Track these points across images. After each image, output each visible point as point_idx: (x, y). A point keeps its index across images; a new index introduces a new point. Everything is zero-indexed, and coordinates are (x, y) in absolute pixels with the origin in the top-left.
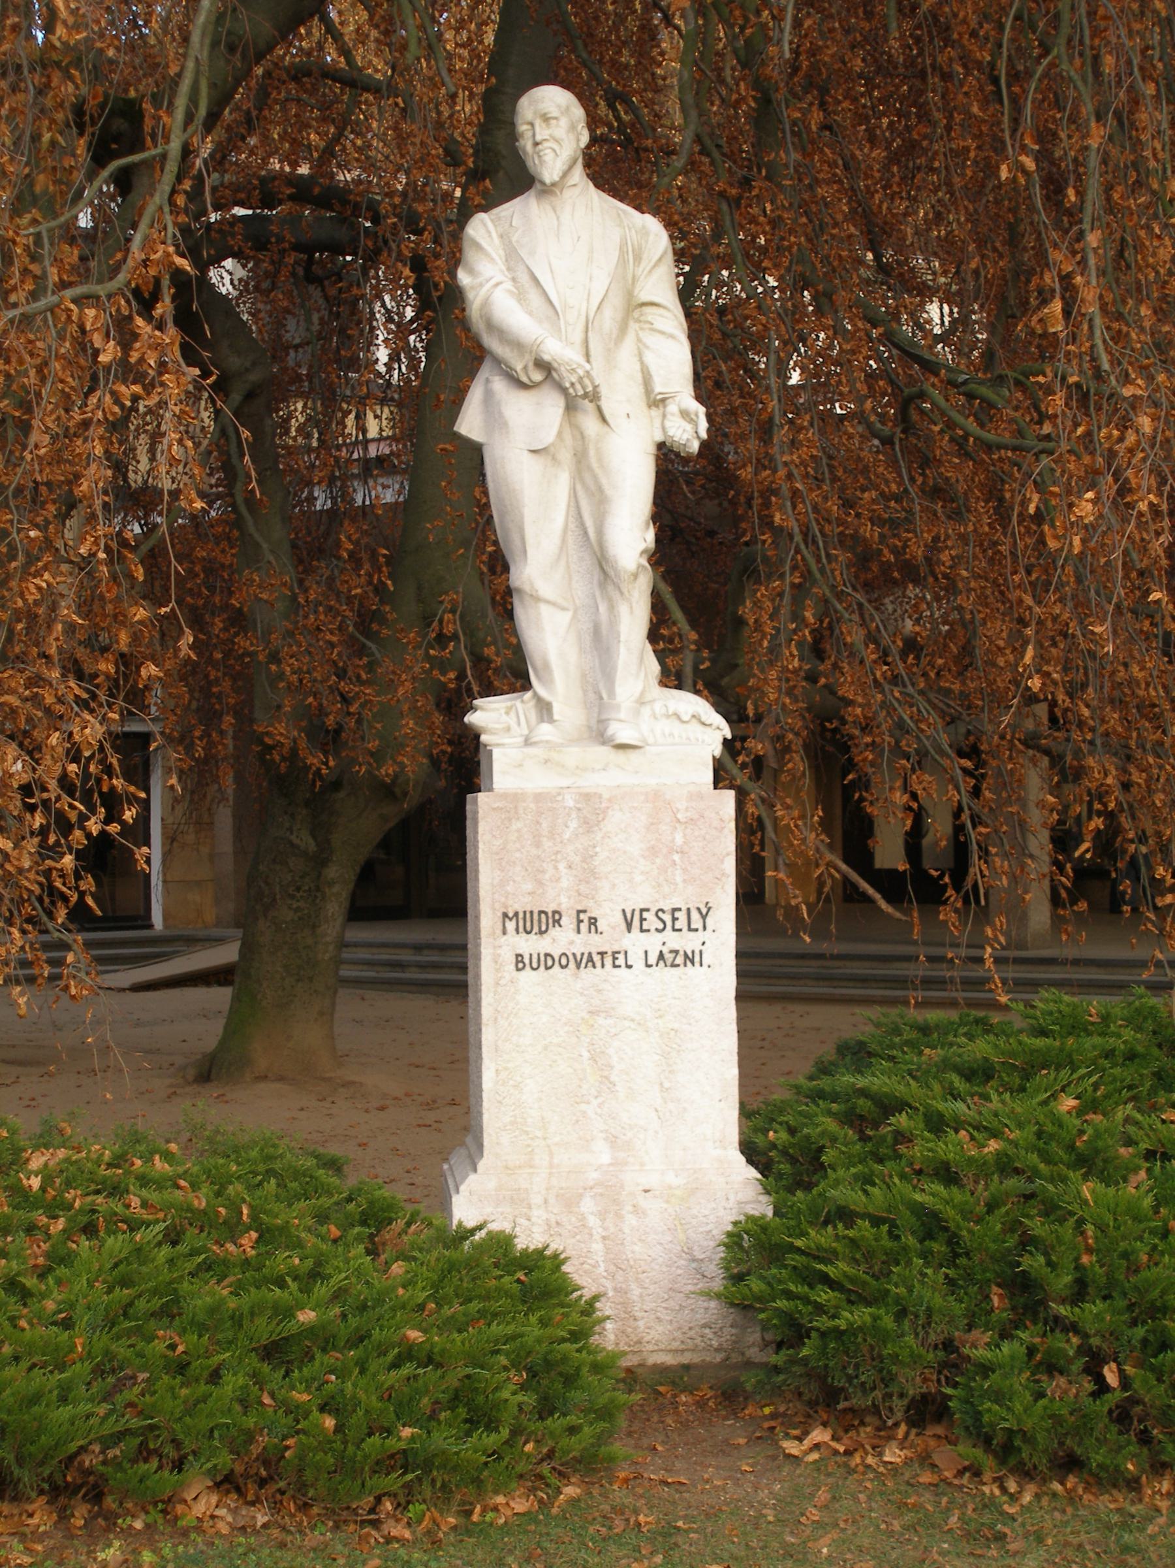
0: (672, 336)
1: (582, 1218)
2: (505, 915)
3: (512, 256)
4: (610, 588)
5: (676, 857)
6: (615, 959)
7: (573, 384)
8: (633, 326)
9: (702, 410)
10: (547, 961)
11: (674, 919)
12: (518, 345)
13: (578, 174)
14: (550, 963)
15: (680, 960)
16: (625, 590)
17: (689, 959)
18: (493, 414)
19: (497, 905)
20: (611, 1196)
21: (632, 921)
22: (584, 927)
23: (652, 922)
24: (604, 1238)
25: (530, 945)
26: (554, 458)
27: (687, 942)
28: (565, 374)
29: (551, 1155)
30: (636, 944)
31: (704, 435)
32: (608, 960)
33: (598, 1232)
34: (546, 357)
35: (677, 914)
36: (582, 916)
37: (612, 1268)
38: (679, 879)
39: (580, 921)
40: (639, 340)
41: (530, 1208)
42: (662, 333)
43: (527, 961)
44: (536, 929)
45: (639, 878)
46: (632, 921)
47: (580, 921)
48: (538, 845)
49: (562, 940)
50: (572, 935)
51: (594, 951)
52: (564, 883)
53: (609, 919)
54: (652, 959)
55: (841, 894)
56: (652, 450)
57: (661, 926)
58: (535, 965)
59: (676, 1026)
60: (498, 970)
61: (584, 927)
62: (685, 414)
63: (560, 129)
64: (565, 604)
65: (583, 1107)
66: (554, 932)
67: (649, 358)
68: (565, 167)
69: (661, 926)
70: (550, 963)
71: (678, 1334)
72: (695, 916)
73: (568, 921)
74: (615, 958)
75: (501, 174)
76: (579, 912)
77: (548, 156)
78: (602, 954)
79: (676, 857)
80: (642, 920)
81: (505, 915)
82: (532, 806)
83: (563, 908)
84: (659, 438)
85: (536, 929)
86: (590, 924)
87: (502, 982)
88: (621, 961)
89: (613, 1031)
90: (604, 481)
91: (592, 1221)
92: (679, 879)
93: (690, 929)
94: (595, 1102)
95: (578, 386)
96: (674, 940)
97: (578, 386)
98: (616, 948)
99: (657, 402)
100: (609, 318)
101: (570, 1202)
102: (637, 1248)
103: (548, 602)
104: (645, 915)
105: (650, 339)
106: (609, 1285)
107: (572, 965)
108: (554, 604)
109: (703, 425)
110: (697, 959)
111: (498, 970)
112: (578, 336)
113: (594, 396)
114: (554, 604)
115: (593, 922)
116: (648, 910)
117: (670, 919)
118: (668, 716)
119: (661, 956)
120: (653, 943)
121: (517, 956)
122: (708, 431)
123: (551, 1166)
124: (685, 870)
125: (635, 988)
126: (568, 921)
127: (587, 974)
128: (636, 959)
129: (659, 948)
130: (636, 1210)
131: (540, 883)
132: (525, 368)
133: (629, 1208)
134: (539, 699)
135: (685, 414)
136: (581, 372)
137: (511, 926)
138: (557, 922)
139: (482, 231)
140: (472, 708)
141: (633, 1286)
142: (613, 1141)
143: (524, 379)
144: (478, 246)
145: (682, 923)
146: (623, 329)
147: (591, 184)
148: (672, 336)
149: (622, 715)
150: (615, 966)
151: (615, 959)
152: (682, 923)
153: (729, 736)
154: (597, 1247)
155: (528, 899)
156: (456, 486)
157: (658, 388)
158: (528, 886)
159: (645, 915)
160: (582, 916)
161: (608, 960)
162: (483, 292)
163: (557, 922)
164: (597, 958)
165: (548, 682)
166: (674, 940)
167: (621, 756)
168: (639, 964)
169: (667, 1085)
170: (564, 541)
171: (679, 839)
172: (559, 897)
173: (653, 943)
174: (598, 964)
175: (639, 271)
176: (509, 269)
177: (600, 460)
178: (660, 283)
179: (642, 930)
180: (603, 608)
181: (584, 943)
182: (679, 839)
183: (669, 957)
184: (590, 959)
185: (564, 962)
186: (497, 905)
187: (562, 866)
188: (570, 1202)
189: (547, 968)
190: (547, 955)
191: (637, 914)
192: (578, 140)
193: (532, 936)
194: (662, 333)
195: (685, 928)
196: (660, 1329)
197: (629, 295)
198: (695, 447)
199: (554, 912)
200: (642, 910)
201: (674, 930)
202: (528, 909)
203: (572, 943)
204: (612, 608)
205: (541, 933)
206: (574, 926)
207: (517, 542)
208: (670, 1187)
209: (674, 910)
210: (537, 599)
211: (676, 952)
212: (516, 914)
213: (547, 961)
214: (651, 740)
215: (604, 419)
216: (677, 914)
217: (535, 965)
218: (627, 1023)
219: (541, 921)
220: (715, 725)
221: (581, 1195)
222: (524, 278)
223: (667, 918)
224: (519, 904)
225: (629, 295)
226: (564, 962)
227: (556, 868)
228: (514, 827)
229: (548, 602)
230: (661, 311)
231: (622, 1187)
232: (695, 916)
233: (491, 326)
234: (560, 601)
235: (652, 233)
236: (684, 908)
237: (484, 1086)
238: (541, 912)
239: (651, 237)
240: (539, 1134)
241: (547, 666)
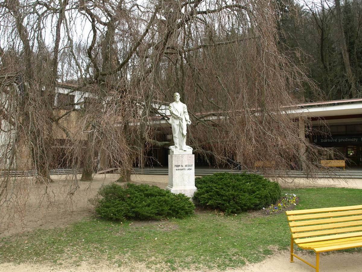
10: (179, 170)
21: (186, 166)
25: (177, 168)
27: (191, 168)
46: (186, 166)
49: (180, 168)
74: (184, 169)
96: (189, 168)
109: (191, 123)
117: (189, 166)
120: (188, 168)
125: (186, 172)
126: (180, 166)
127: (182, 171)
166: (189, 168)
173: (188, 168)
181: (182, 168)
213: (179, 170)
219: (178, 166)
235: (185, 106)
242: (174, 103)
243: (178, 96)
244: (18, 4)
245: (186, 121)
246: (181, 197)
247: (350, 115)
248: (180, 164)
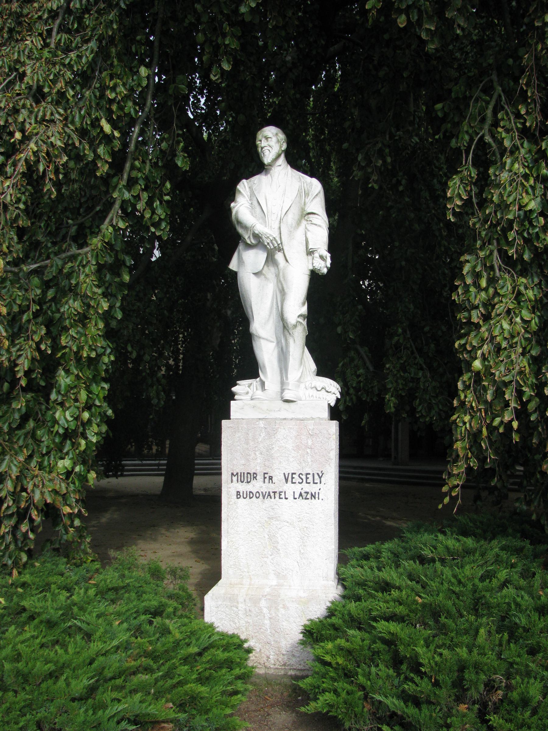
0: (320, 226)
1: (261, 609)
2: (232, 474)
3: (253, 194)
4: (286, 332)
5: (309, 450)
6: (280, 495)
7: (268, 243)
8: (304, 223)
9: (329, 255)
10: (250, 495)
11: (307, 478)
12: (246, 228)
13: (282, 160)
14: (251, 496)
15: (309, 496)
16: (291, 332)
17: (313, 496)
18: (241, 261)
19: (229, 470)
20: (274, 601)
21: (288, 478)
22: (267, 480)
23: (297, 479)
24: (270, 618)
25: (243, 487)
26: (265, 277)
27: (312, 488)
28: (264, 239)
29: (251, 579)
30: (290, 489)
31: (329, 266)
32: (277, 495)
33: (267, 616)
34: (256, 232)
35: (308, 476)
36: (266, 475)
37: (274, 632)
38: (309, 460)
39: (265, 478)
40: (306, 228)
41: (238, 603)
42: (316, 225)
43: (241, 494)
44: (246, 481)
45: (291, 459)
46: (288, 478)
47: (265, 478)
48: (247, 443)
49: (257, 486)
50: (261, 483)
51: (271, 491)
52: (259, 461)
53: (278, 477)
54: (297, 496)
55: (387, 466)
56: (308, 273)
57: (301, 481)
58: (245, 496)
59: (307, 525)
60: (229, 498)
61: (267, 480)
62: (321, 257)
63: (273, 142)
64: (272, 340)
65: (265, 559)
66: (253, 482)
67: (309, 235)
68: (274, 157)
69: (301, 481)
70: (251, 496)
71: (302, 662)
72: (316, 477)
73: (260, 477)
74: (280, 495)
75: (256, 166)
76: (265, 474)
77: (267, 153)
78: (275, 492)
79: (309, 450)
80: (292, 478)
81: (232, 474)
82: (245, 426)
83: (257, 472)
84: (311, 268)
85: (246, 481)
86: (270, 479)
87: (231, 503)
88: (283, 496)
89: (279, 526)
90: (285, 286)
91: (265, 610)
92: (309, 460)
93: (314, 483)
94: (270, 557)
95: (271, 245)
96: (306, 488)
97: (271, 245)
98: (281, 490)
99: (310, 253)
100: (291, 218)
101: (255, 601)
102: (284, 623)
103: (264, 339)
104: (294, 476)
105: (310, 227)
106: (272, 639)
107: (261, 497)
108: (267, 340)
109: (329, 262)
110: (317, 496)
111: (229, 498)
112: (276, 226)
113: (280, 249)
114: (267, 340)
115: (271, 478)
116: (295, 474)
117: (305, 478)
118: (312, 388)
119: (301, 495)
120: (298, 488)
121: (238, 492)
122: (331, 264)
123: (250, 584)
124: (312, 456)
125: (289, 508)
126: (260, 477)
127: (268, 501)
128: (290, 495)
129: (300, 491)
130: (285, 607)
131: (248, 460)
132: (249, 237)
133: (281, 606)
134: (261, 380)
135: (321, 257)
136: (271, 238)
137: (235, 479)
138: (255, 478)
139: (242, 186)
140: (236, 385)
141: (282, 640)
142: (278, 575)
143: (249, 242)
144: (240, 192)
145: (310, 480)
146: (299, 223)
147: (289, 166)
148: (320, 226)
149: (290, 387)
150: (280, 498)
151: (280, 495)
152: (310, 480)
153: (339, 397)
154: (267, 622)
155: (242, 467)
156: (229, 292)
157: (310, 247)
158: (243, 462)
159: (294, 476)
160: (266, 475)
161: (277, 495)
162: (236, 209)
163: (255, 478)
164: (272, 494)
165: (265, 373)
166: (306, 488)
167: (286, 405)
168: (291, 498)
169: (302, 551)
170: (271, 312)
171: (310, 443)
172: (257, 467)
173: (298, 488)
174: (273, 497)
175: (307, 200)
176: (250, 200)
177: (284, 277)
178: (317, 204)
179: (292, 483)
180: (283, 341)
181: (266, 487)
182: (310, 443)
183: (304, 495)
184: (269, 495)
185: (258, 495)
186: (229, 470)
187: (257, 453)
188: (255, 601)
189: (250, 498)
190: (250, 492)
191: (290, 475)
192: (281, 147)
193: (244, 483)
194: (316, 225)
195: (312, 482)
196: (294, 659)
197: (303, 210)
198: (325, 271)
199: (254, 473)
200: (293, 474)
201: (307, 483)
202: (242, 471)
203: (261, 487)
204: (286, 340)
205: (248, 482)
206: (262, 480)
207: (250, 313)
208: (301, 597)
209: (307, 474)
210: (260, 338)
211: (307, 493)
212: (237, 474)
213: (250, 495)
214: (303, 398)
215: (287, 261)
216: (308, 476)
217: (245, 496)
218: (285, 524)
219: (247, 477)
220: (333, 392)
221: (260, 599)
222: (255, 203)
223: (304, 477)
224: (239, 469)
225: (303, 210)
226: (258, 495)
227: (255, 454)
228: (237, 435)
229: (264, 339)
230: (316, 216)
231: (279, 596)
232: (316, 477)
233: (239, 222)
234: (269, 338)
235: (315, 186)
236: (311, 473)
237: (222, 548)
238: (248, 473)
239: (313, 187)
240: (245, 570)
241: (264, 366)
242: (259, 180)
243: (271, 142)
244: (544, 13)
245: (310, 253)
246: (234, 649)
247: (340, 435)
248: (260, 471)
